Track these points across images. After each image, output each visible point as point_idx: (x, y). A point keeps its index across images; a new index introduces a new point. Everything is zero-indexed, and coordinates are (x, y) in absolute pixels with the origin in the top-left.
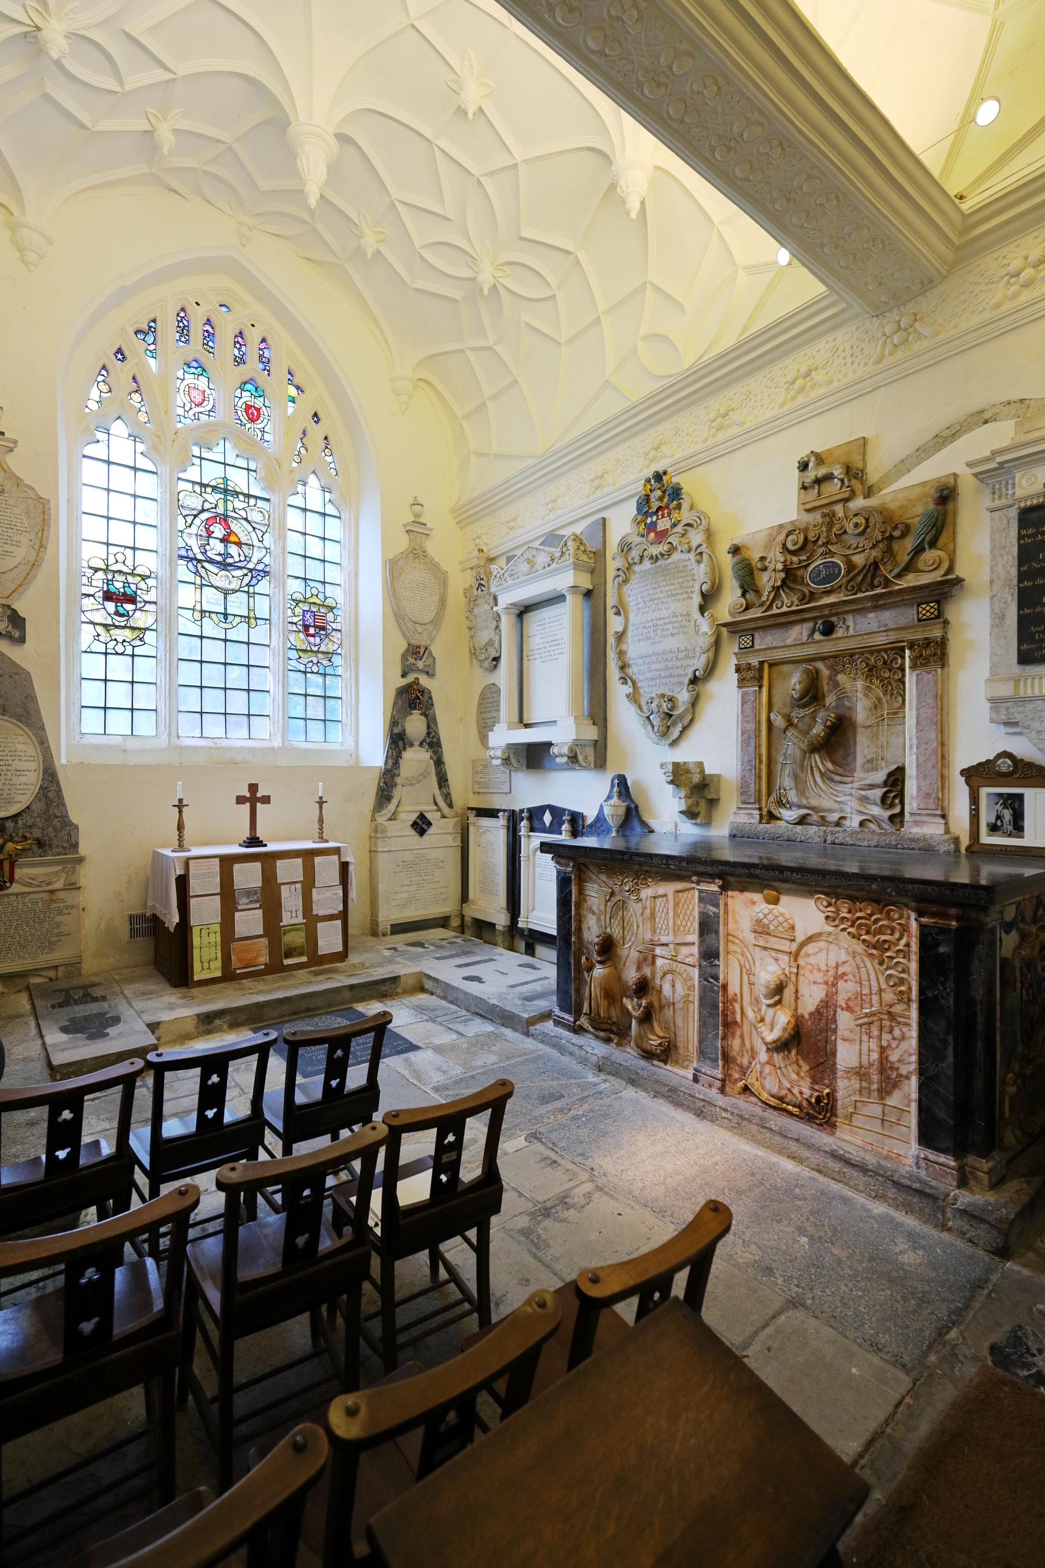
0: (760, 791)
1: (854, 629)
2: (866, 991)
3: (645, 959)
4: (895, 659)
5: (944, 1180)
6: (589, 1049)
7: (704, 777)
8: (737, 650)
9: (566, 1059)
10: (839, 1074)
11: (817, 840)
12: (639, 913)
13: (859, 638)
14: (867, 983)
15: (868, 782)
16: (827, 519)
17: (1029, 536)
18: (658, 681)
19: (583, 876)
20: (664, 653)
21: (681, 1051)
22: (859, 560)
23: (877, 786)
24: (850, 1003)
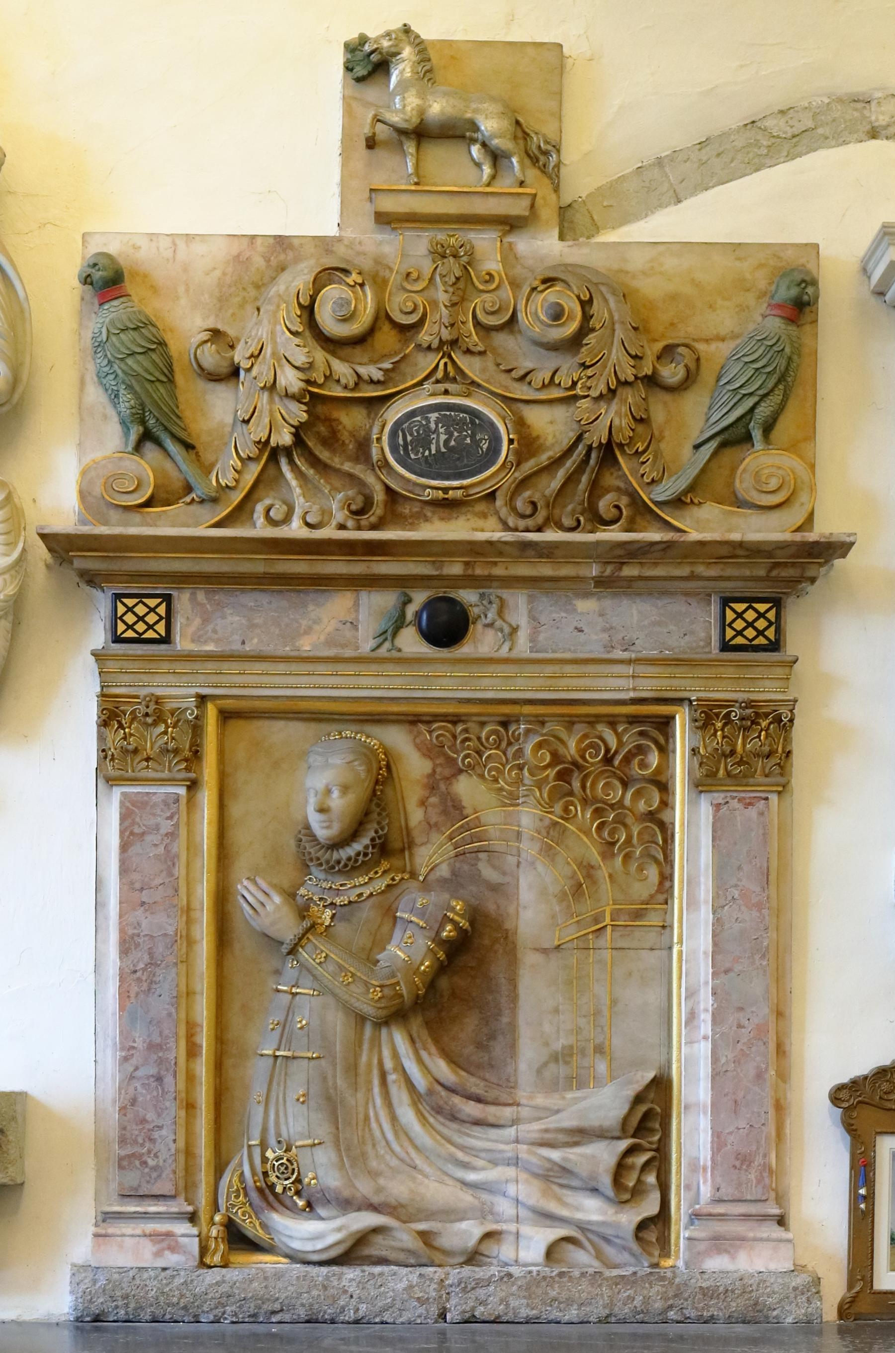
0: (189, 1153)
1: (533, 639)
4: (640, 750)
8: (99, 638)
13: (549, 670)
15: (567, 1120)
23: (600, 1134)
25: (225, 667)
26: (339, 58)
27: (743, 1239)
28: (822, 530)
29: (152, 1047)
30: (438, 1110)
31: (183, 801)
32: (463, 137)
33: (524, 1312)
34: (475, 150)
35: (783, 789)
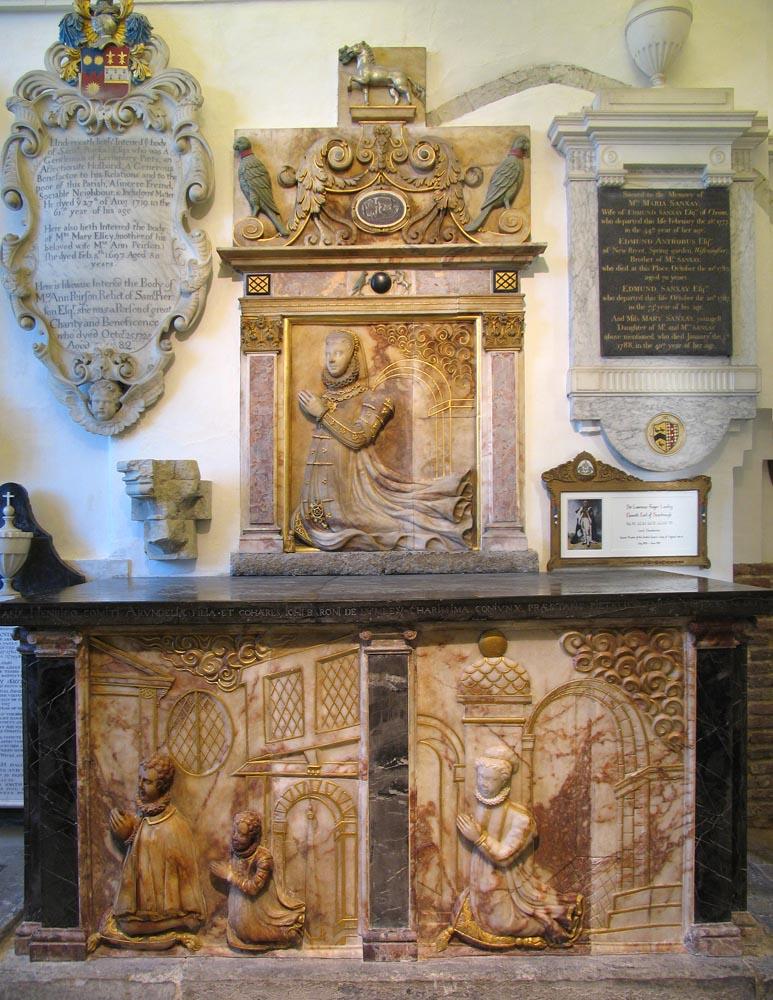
1: (417, 289)
2: (628, 749)
4: (462, 334)
7: (200, 484)
8: (241, 294)
10: (594, 869)
12: (236, 710)
13: (424, 302)
14: (629, 739)
16: (383, 139)
17: (610, 217)
18: (100, 329)
20: (116, 283)
22: (424, 201)
24: (609, 771)
25: (293, 304)
26: (337, 56)
27: (506, 537)
28: (535, 240)
29: (263, 461)
30: (382, 486)
31: (275, 359)
32: (387, 86)
33: (417, 569)
34: (392, 91)
35: (521, 350)
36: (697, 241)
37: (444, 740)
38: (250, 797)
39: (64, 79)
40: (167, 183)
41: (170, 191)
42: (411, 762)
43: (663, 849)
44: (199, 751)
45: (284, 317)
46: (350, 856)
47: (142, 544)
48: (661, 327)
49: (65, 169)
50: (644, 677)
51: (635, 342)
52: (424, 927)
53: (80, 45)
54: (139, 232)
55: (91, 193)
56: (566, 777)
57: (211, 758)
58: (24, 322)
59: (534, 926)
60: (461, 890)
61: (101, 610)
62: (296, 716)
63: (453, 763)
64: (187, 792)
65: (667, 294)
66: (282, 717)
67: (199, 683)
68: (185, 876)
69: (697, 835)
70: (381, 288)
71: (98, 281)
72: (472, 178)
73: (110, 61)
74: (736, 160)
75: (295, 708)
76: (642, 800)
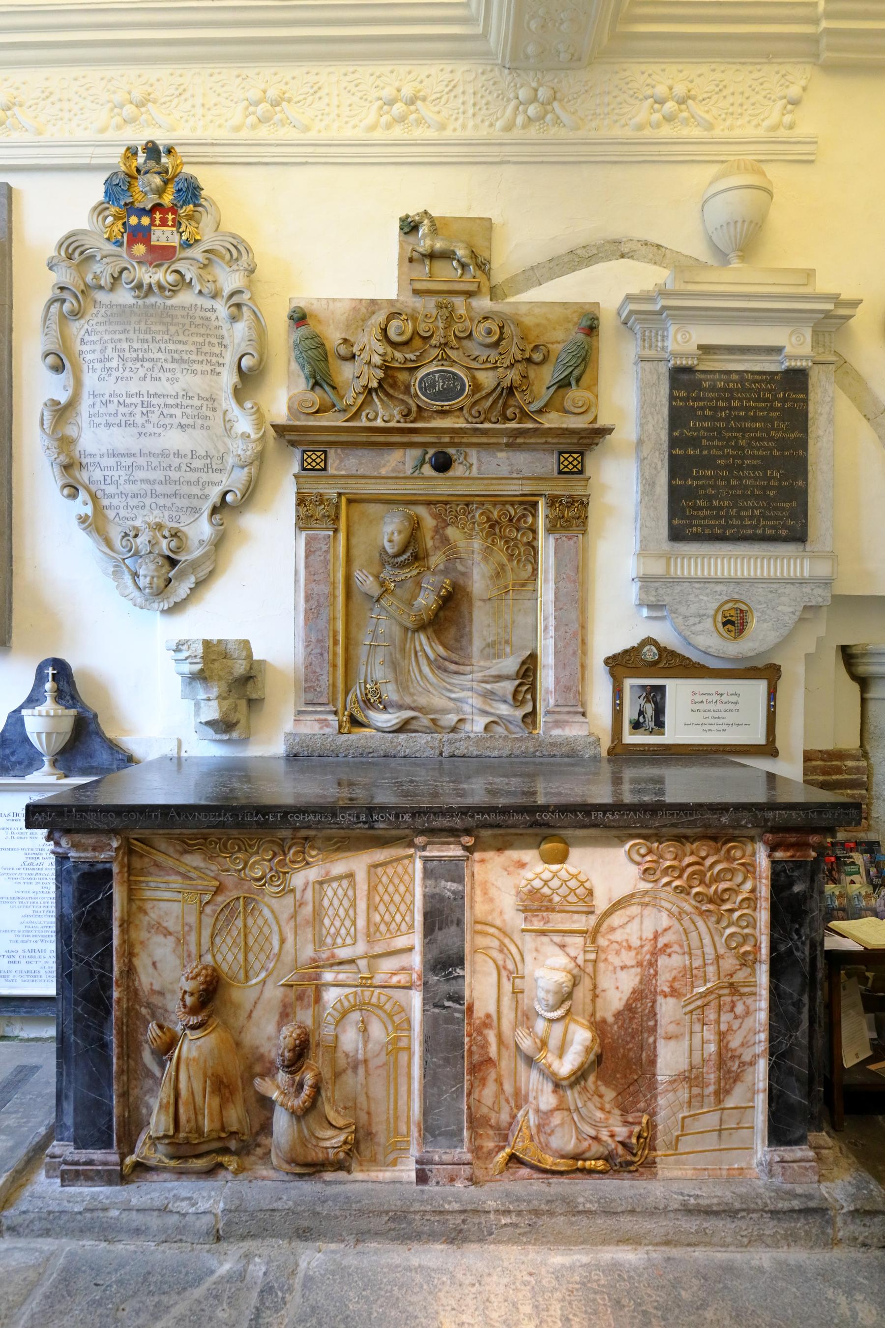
0: (334, 685)
1: (479, 469)
2: (697, 963)
3: (300, 998)
4: (524, 516)
5: (804, 1180)
6: (184, 1206)
8: (296, 468)
9: (124, 1247)
10: (661, 1088)
11: (429, 752)
12: (284, 916)
13: (486, 482)
15: (493, 672)
17: (681, 399)
18: (148, 501)
19: (137, 863)
20: (164, 454)
21: (381, 1138)
22: (487, 379)
23: (508, 678)
24: (676, 985)
26: (397, 225)
28: (602, 422)
33: (475, 753)
34: (455, 263)
36: (773, 425)
37: (502, 948)
38: (298, 1009)
39: (108, 239)
40: (218, 352)
41: (221, 360)
42: (467, 972)
43: (735, 1068)
44: (246, 959)
45: (340, 494)
46: (403, 1070)
47: (192, 722)
48: (733, 512)
49: (110, 332)
50: (713, 888)
51: (703, 527)
52: (480, 1148)
53: (126, 204)
54: (190, 402)
55: (137, 359)
56: (631, 990)
57: (257, 966)
58: (66, 491)
59: (596, 1149)
60: (519, 1107)
61: (141, 813)
62: (348, 923)
63: (511, 973)
64: (232, 1003)
65: (740, 479)
66: (332, 924)
67: (246, 887)
68: (228, 1095)
69: (771, 1055)
70: (443, 464)
71: (145, 451)
72: (537, 357)
73: (158, 222)
74: (816, 343)
75: (347, 914)
76: (711, 1015)
